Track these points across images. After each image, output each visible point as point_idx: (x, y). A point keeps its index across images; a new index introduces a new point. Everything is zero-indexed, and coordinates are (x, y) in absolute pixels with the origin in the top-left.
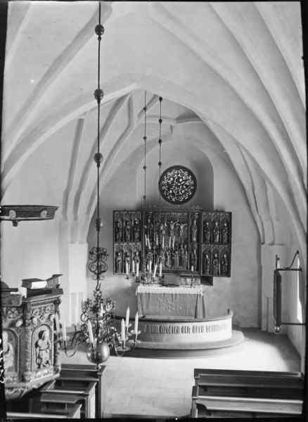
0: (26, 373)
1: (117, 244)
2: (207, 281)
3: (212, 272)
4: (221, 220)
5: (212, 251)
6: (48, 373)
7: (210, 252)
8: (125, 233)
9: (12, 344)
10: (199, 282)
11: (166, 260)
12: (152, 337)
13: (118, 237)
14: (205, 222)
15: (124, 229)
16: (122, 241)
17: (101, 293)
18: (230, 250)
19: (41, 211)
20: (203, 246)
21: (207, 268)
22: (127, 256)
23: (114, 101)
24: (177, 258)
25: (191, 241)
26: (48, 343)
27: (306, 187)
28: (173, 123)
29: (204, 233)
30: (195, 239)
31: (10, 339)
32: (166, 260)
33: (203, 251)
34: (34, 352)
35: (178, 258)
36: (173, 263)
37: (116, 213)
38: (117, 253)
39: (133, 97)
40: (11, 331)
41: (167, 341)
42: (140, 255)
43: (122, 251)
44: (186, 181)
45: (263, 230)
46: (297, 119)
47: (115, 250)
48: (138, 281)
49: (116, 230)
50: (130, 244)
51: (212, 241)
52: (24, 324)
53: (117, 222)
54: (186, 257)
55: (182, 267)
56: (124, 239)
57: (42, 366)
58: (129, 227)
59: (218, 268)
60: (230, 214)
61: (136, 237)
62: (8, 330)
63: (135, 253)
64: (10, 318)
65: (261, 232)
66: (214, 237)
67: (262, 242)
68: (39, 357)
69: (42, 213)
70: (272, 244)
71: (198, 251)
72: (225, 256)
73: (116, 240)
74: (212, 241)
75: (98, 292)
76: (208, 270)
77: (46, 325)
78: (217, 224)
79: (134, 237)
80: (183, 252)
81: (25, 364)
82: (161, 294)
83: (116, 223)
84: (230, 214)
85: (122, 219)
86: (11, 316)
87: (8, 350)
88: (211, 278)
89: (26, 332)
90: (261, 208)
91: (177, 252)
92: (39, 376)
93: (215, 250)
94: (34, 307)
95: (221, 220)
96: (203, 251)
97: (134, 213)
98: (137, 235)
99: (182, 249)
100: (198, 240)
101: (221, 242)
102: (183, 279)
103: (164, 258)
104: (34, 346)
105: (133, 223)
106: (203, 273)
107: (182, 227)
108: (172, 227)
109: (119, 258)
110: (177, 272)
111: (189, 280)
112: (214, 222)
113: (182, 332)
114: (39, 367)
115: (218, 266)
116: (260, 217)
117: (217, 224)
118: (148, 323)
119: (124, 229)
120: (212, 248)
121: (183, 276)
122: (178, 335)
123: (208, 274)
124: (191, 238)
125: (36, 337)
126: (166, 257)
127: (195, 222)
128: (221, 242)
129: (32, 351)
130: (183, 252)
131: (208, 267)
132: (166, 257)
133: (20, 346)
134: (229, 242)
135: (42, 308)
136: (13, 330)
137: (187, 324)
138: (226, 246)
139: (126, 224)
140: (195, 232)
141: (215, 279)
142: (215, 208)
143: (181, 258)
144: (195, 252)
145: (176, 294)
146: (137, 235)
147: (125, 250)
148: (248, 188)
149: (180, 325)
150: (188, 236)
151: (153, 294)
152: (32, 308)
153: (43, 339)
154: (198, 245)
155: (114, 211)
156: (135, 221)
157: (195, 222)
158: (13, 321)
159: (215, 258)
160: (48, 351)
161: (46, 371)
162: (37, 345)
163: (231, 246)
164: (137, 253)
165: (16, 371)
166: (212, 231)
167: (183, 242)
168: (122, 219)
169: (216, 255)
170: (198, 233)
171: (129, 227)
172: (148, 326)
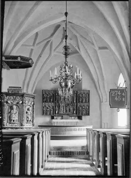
0: (23, 122)
1: (43, 103)
2: (80, 118)
3: (82, 114)
5: (82, 106)
6: (30, 125)
7: (81, 106)
8: (47, 99)
9: (18, 111)
10: (77, 118)
11: (64, 110)
13: (44, 100)
14: (79, 95)
15: (47, 98)
17: (67, 62)
18: (89, 105)
19: (29, 60)
20: (78, 104)
21: (80, 112)
22: (48, 108)
23: (56, 25)
24: (68, 109)
27: (129, 50)
30: (75, 102)
32: (64, 110)
33: (78, 106)
35: (68, 109)
36: (66, 111)
37: (44, 91)
38: (44, 107)
40: (18, 106)
41: (67, 134)
42: (53, 108)
43: (46, 106)
49: (43, 98)
51: (82, 102)
52: (22, 103)
53: (44, 95)
54: (71, 109)
55: (70, 113)
56: (46, 101)
58: (48, 97)
59: (84, 112)
60: (89, 91)
61: (51, 101)
62: (16, 105)
63: (51, 107)
64: (17, 100)
65: (101, 98)
68: (28, 118)
71: (76, 106)
72: (87, 107)
73: (43, 102)
74: (82, 102)
75: (66, 62)
76: (81, 113)
79: (51, 100)
80: (70, 107)
82: (62, 122)
83: (43, 95)
85: (46, 93)
87: (16, 112)
88: (81, 117)
89: (23, 106)
91: (68, 107)
92: (27, 125)
93: (83, 105)
94: (27, 97)
95: (85, 93)
96: (78, 106)
97: (50, 91)
98: (52, 100)
100: (76, 102)
101: (86, 102)
102: (70, 117)
103: (63, 109)
104: (26, 113)
105: (50, 95)
106: (79, 115)
109: (45, 109)
110: (68, 115)
112: (83, 95)
113: (74, 130)
115: (85, 112)
116: (101, 92)
119: (47, 98)
120: (82, 104)
122: (72, 132)
123: (80, 115)
126: (64, 109)
128: (86, 102)
129: (25, 115)
130: (70, 107)
131: (81, 112)
132: (64, 109)
134: (89, 101)
135: (29, 99)
139: (48, 96)
141: (83, 117)
142: (83, 89)
143: (69, 109)
144: (75, 106)
145: (68, 122)
146: (52, 100)
147: (47, 106)
148: (96, 80)
149: (73, 128)
150: (72, 100)
151: (59, 122)
152: (26, 97)
153: (29, 111)
154: (77, 104)
155: (43, 90)
156: (51, 95)
158: (18, 102)
159: (83, 108)
162: (27, 113)
163: (89, 104)
164: (52, 107)
165: (19, 121)
166: (82, 98)
167: (70, 103)
168: (46, 93)
171: (48, 97)
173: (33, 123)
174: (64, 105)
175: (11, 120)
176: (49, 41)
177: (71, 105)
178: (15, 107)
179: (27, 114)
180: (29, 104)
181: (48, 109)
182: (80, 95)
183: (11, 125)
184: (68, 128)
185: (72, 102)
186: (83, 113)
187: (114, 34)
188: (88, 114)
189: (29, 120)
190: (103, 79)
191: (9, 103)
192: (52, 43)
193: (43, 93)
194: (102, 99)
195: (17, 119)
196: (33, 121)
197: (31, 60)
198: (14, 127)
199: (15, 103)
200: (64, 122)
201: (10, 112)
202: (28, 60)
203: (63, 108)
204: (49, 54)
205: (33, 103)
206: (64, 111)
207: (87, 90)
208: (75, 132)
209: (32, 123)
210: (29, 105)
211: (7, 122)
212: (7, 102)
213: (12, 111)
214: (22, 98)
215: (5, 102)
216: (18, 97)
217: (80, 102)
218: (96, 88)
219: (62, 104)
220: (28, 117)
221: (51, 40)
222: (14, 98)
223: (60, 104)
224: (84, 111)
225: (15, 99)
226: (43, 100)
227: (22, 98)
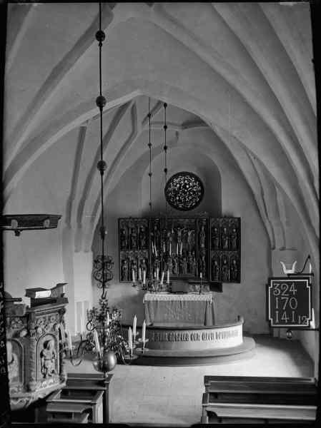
0: (31, 383)
1: (122, 252)
2: (216, 287)
9: (17, 354)
10: (208, 288)
13: (123, 245)
14: (213, 228)
19: (43, 221)
20: (211, 252)
22: (133, 264)
24: (185, 266)
25: (200, 247)
26: (53, 353)
28: (177, 130)
30: (203, 246)
36: (181, 270)
38: (123, 261)
40: (17, 342)
41: (176, 348)
42: (146, 263)
44: (193, 187)
49: (122, 238)
52: (28, 334)
56: (130, 247)
57: (47, 375)
58: (135, 235)
60: (239, 219)
61: (143, 245)
62: (12, 340)
63: (141, 261)
67: (272, 247)
69: (46, 221)
70: (283, 249)
73: (121, 248)
74: (221, 247)
76: (217, 277)
77: (51, 335)
79: (140, 243)
83: (121, 231)
84: (239, 219)
86: (15, 326)
87: (13, 360)
89: (30, 342)
90: (271, 215)
91: (185, 259)
92: (45, 386)
97: (139, 220)
98: (143, 243)
101: (230, 248)
106: (213, 279)
107: (189, 234)
108: (180, 234)
111: (197, 287)
118: (157, 331)
127: (203, 229)
128: (230, 248)
129: (37, 362)
130: (191, 259)
132: (173, 264)
133: (25, 356)
135: (47, 318)
136: (16, 339)
139: (132, 232)
140: (203, 238)
141: (224, 286)
143: (188, 265)
144: (203, 258)
145: (184, 302)
146: (143, 243)
148: (256, 192)
149: (189, 333)
153: (48, 349)
154: (207, 252)
155: (119, 219)
156: (141, 228)
157: (203, 229)
159: (223, 264)
160: (53, 360)
161: (51, 381)
162: (42, 355)
164: (144, 261)
165: (21, 380)
169: (225, 262)
172: (156, 334)
173: (60, 374)
179: (43, 359)
180: (48, 331)
182: (216, 230)
184: (177, 333)
185: (195, 245)
186: (223, 276)
187: (273, 138)
188: (236, 278)
193: (121, 225)
194: (274, 241)
196: (61, 371)
197: (48, 221)
200: (172, 301)
202: (39, 221)
204: (131, 131)
206: (176, 271)
207: (235, 218)
208: (194, 342)
209: (58, 376)
210: (48, 334)
214: (27, 322)
216: (17, 320)
217: (216, 248)
218: (258, 210)
220: (44, 365)
224: (226, 270)
226: (121, 243)
227: (27, 322)
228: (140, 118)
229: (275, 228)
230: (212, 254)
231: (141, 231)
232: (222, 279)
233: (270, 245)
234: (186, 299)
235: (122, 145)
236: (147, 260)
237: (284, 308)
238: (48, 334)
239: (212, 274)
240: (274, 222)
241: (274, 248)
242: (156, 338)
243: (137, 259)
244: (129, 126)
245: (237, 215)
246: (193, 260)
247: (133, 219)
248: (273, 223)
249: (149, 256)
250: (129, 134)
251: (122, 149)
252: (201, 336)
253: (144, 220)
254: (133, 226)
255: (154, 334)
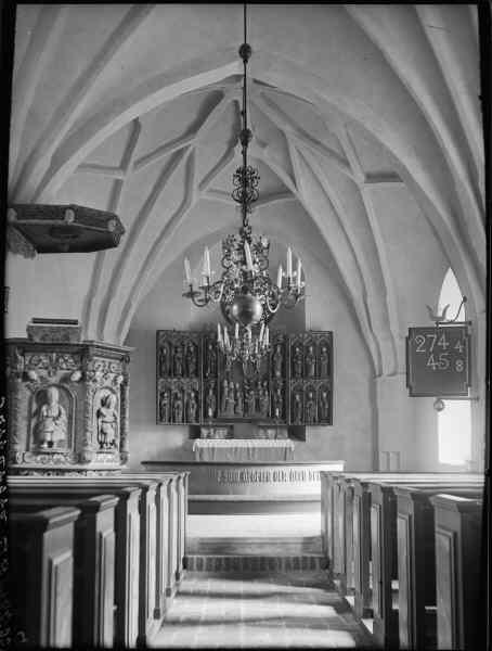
0: (86, 448)
1: (162, 380)
2: (297, 434)
4: (318, 343)
5: (304, 388)
7: (301, 390)
8: (175, 364)
9: (64, 407)
11: (236, 406)
12: (229, 486)
13: (163, 369)
14: (293, 348)
16: (170, 375)
19: (109, 220)
22: (176, 398)
24: (252, 401)
25: (274, 375)
29: (293, 363)
30: (278, 374)
31: (60, 401)
32: (236, 406)
34: (95, 424)
38: (162, 394)
39: (197, 152)
40: (66, 390)
41: (249, 493)
42: (196, 397)
43: (170, 390)
45: (379, 355)
46: (469, 86)
47: (159, 388)
48: (195, 433)
49: (161, 360)
50: (182, 380)
52: (83, 379)
54: (266, 400)
56: (172, 373)
60: (331, 333)
61: (191, 370)
62: (58, 386)
63: (189, 395)
64: (62, 369)
65: (376, 363)
66: (306, 368)
67: (377, 373)
68: (103, 432)
70: (394, 374)
73: (160, 373)
78: (311, 349)
80: (261, 393)
81: (85, 435)
82: (231, 449)
83: (160, 349)
84: (331, 333)
89: (85, 389)
90: (376, 323)
91: (252, 393)
95: (318, 343)
99: (260, 387)
100: (284, 374)
101: (318, 375)
102: (262, 431)
106: (292, 421)
111: (270, 432)
114: (102, 447)
117: (311, 349)
118: (223, 467)
121: (263, 427)
124: (274, 373)
125: (98, 405)
127: (279, 350)
128: (318, 375)
129: (93, 424)
130: (261, 393)
132: (236, 400)
136: (66, 385)
137: (277, 469)
138: (326, 380)
139: (176, 352)
141: (309, 432)
143: (257, 401)
144: (279, 391)
145: (254, 449)
148: (356, 293)
149: (271, 470)
153: (108, 407)
154: (284, 382)
155: (158, 332)
157: (279, 350)
159: (308, 399)
161: (110, 456)
162: (99, 414)
164: (193, 395)
165: (70, 446)
168: (170, 344)
169: (311, 395)
170: (283, 365)
172: (223, 473)
173: (121, 451)
174: (237, 386)
175: (42, 442)
176: (179, 153)
177: (262, 386)
178: (55, 393)
179: (100, 420)
181: (180, 402)
183: (39, 458)
184: (253, 470)
185: (267, 374)
187: (422, 121)
188: (326, 419)
189: (109, 439)
190: (381, 288)
191: (32, 381)
192: (191, 159)
195: (63, 436)
196: (122, 446)
198: (51, 465)
199: (54, 380)
201: (38, 412)
203: (235, 395)
204: (182, 198)
205: (121, 379)
209: (117, 452)
210: (107, 388)
211: (27, 450)
212: (26, 377)
213: (44, 408)
215: (18, 376)
219: (232, 384)
220: (102, 431)
221: (191, 148)
222: (51, 360)
223: (222, 383)
225: (55, 366)
228: (198, 177)
229: (381, 344)
230: (292, 384)
231: (189, 351)
232: (305, 421)
233: (375, 373)
234: (256, 446)
235: (166, 221)
236: (197, 393)
237: (431, 350)
238: (107, 388)
239: (292, 414)
240: (380, 335)
241: (380, 375)
242: (223, 477)
243: (183, 391)
244: (181, 189)
245: (327, 328)
246: (264, 394)
247: (179, 332)
248: (379, 338)
249: (200, 387)
250: (179, 204)
251: (168, 226)
252: (288, 475)
253: (195, 335)
254: (179, 344)
255: (220, 472)
